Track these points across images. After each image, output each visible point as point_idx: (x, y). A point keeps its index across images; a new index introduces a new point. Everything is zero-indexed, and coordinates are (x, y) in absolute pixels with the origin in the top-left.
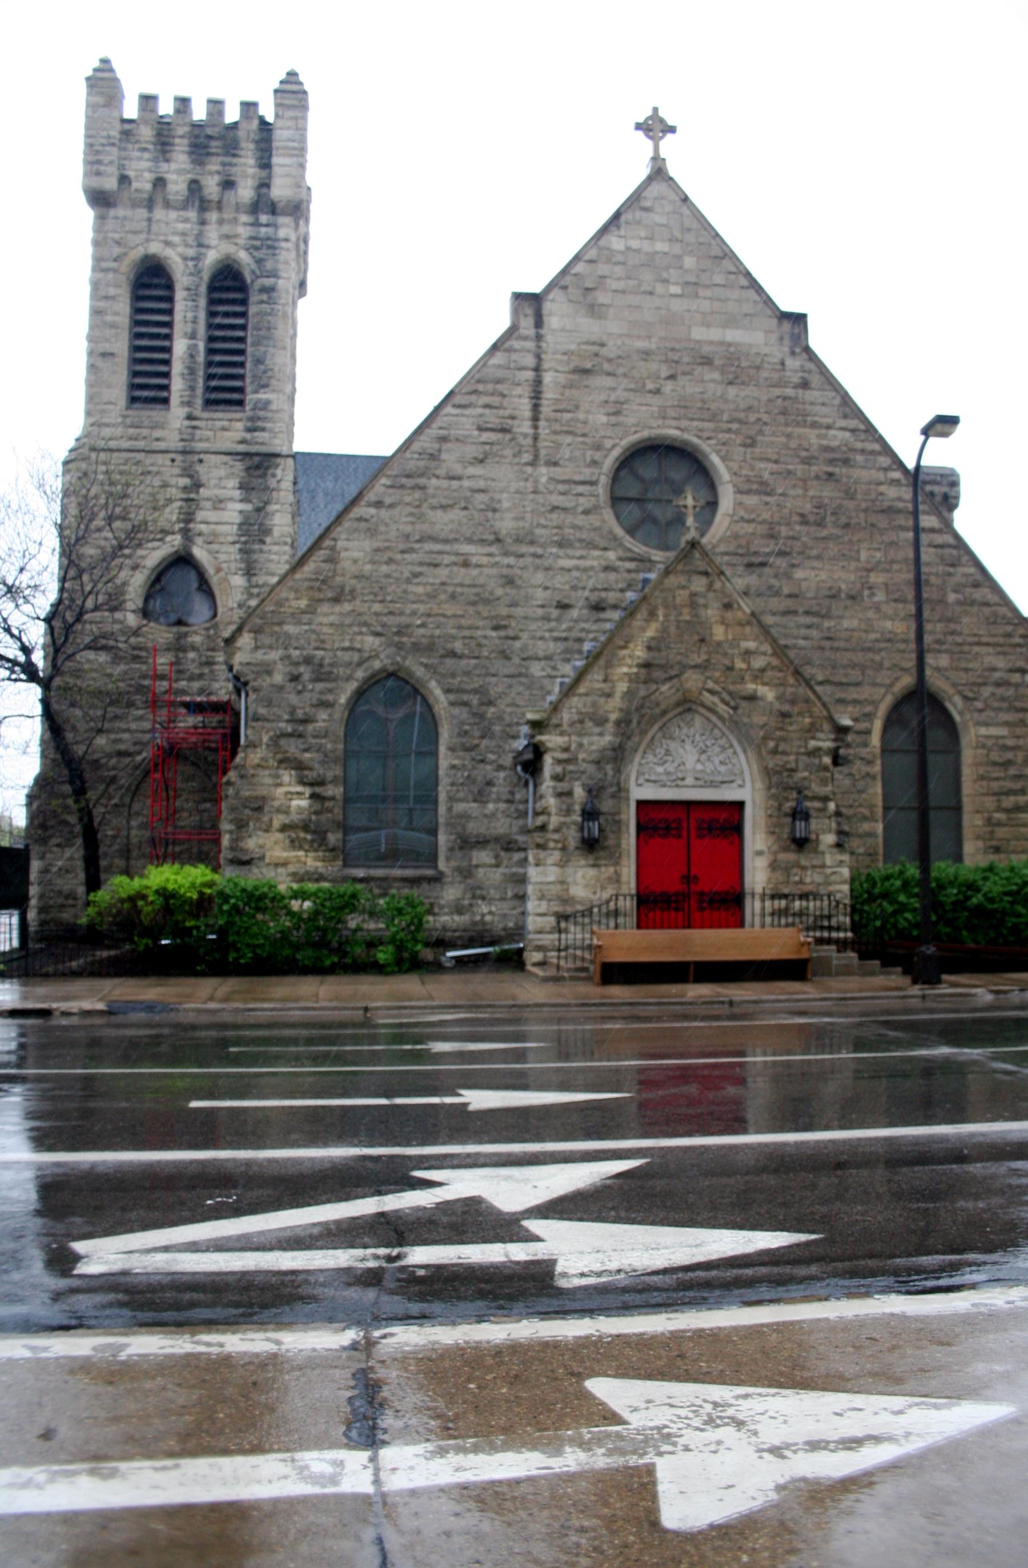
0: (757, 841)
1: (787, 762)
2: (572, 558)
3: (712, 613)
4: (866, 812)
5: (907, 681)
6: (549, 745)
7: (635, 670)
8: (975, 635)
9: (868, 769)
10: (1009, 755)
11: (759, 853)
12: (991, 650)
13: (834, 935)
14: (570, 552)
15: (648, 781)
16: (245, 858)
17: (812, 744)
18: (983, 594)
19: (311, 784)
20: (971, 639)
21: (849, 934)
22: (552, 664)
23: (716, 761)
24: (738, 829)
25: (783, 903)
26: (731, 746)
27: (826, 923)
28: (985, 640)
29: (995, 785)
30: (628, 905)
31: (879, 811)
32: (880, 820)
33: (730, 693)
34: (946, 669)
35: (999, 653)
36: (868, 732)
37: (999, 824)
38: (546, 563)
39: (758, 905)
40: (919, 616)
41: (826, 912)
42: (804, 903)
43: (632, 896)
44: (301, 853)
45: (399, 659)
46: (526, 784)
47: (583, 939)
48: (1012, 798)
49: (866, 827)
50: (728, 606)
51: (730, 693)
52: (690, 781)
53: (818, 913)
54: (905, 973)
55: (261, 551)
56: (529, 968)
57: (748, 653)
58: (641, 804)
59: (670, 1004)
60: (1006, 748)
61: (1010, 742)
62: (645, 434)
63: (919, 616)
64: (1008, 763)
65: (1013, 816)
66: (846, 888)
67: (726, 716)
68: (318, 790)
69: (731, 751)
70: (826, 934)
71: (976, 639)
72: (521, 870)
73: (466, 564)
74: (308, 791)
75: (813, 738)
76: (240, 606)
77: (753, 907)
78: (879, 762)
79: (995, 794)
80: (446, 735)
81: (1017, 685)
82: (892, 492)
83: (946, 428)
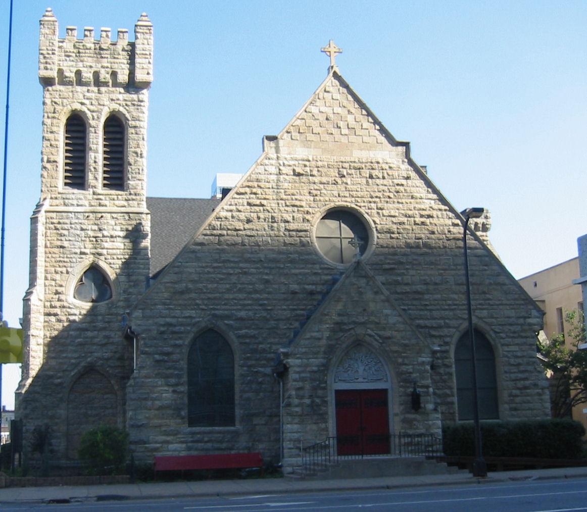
0: (395, 407)
1: (408, 369)
2: (298, 269)
3: (369, 295)
4: (448, 391)
5: (465, 325)
6: (292, 364)
7: (332, 326)
8: (499, 300)
9: (447, 370)
10: (520, 360)
11: (396, 415)
12: (508, 307)
13: (435, 454)
14: (297, 266)
15: (340, 380)
16: (140, 424)
17: (420, 359)
18: (502, 279)
19: (172, 386)
20: (497, 303)
21: (442, 454)
22: (290, 322)
23: (373, 369)
24: (385, 403)
25: (410, 439)
26: (380, 362)
27: (430, 449)
28: (504, 302)
29: (513, 376)
30: (332, 442)
31: (455, 390)
32: (456, 395)
33: (379, 336)
34: (485, 318)
35: (512, 309)
36: (447, 352)
37: (516, 396)
38: (286, 271)
39: (397, 440)
40: (468, 293)
41: (430, 444)
42: (420, 439)
43: (333, 438)
44: (167, 421)
45: (214, 321)
46: (279, 383)
47: (314, 460)
48: (522, 382)
49: (449, 399)
50: (376, 293)
51: (379, 336)
52: (361, 380)
53: (427, 444)
54: (470, 472)
55: (135, 263)
56: (286, 475)
57: (387, 315)
58: (338, 392)
59: (150, 497)
60: (517, 357)
61: (519, 354)
62: (332, 205)
63: (468, 293)
64: (519, 364)
65: (523, 391)
66: (440, 431)
67: (377, 347)
68: (176, 388)
69: (380, 364)
70: (431, 454)
71: (500, 302)
72: (277, 426)
73: (245, 273)
74: (171, 389)
75: (420, 357)
76: (124, 292)
77: (395, 442)
78: (454, 366)
79: (513, 380)
80: (237, 357)
81: (522, 325)
82: (455, 230)
83: (478, 214)
